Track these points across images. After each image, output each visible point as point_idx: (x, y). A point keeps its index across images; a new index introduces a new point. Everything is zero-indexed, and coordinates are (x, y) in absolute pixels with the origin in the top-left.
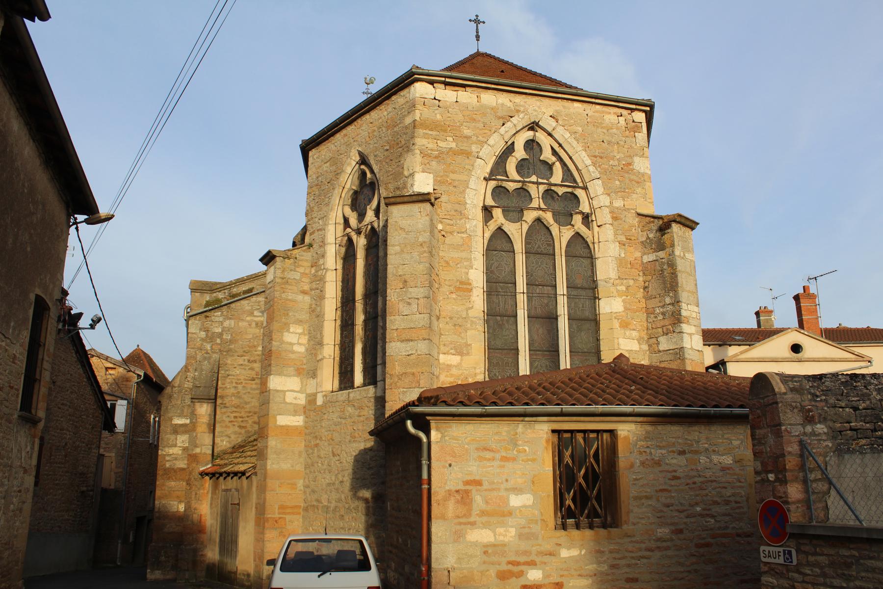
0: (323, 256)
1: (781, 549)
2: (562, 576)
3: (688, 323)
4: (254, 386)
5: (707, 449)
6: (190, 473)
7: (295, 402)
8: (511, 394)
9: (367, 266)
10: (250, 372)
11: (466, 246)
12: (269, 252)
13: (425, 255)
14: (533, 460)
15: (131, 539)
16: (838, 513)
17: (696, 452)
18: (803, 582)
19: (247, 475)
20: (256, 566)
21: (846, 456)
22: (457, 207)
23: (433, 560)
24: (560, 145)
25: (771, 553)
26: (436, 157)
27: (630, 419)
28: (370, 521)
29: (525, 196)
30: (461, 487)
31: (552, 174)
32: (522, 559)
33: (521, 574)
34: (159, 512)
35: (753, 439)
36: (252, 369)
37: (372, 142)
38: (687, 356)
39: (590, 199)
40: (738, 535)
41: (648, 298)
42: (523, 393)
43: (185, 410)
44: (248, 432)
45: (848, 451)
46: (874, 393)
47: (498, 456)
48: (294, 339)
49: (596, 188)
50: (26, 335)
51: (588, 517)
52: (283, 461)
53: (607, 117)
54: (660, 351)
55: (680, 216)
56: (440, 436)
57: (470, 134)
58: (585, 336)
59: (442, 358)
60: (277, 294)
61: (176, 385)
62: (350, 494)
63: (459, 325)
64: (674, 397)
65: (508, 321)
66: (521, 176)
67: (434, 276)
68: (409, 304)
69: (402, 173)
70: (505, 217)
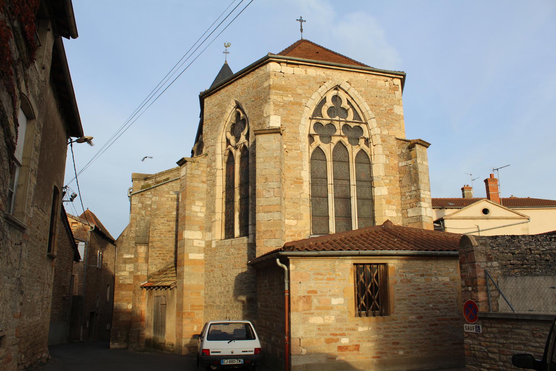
0: (215, 161)
1: (474, 325)
2: (359, 341)
3: (424, 201)
4: (170, 236)
5: (436, 274)
6: (135, 287)
7: (199, 245)
8: (331, 244)
9: (241, 167)
10: (168, 227)
11: (299, 157)
12: (183, 159)
13: (278, 163)
14: (344, 280)
15: (88, 326)
16: (503, 307)
17: (430, 275)
18: (485, 341)
19: (171, 287)
20: (177, 340)
21: (508, 278)
22: (294, 135)
23: (292, 333)
24: (352, 99)
25: (469, 328)
26: (282, 106)
27: (395, 257)
28: (245, 314)
29: (332, 128)
30: (306, 294)
31: (347, 115)
32: (338, 332)
33: (338, 340)
34: (116, 309)
35: (461, 269)
36: (169, 225)
37: (243, 96)
38: (423, 220)
39: (369, 130)
40: (452, 320)
41: (402, 187)
42: (338, 243)
43: (131, 250)
44: (167, 262)
45: (509, 275)
46: (523, 245)
47: (325, 277)
48: (197, 209)
49: (373, 123)
50: (50, 208)
51: (372, 310)
52: (193, 279)
53: (379, 82)
54: (408, 217)
55: (420, 140)
56: (294, 267)
57: (301, 93)
58: (366, 209)
59: (287, 222)
60: (188, 183)
61: (125, 235)
62: (233, 298)
63: (296, 203)
64: (418, 245)
65: (323, 200)
66: (330, 117)
67: (282, 176)
68: (269, 191)
69: (263, 115)
70: (321, 140)
